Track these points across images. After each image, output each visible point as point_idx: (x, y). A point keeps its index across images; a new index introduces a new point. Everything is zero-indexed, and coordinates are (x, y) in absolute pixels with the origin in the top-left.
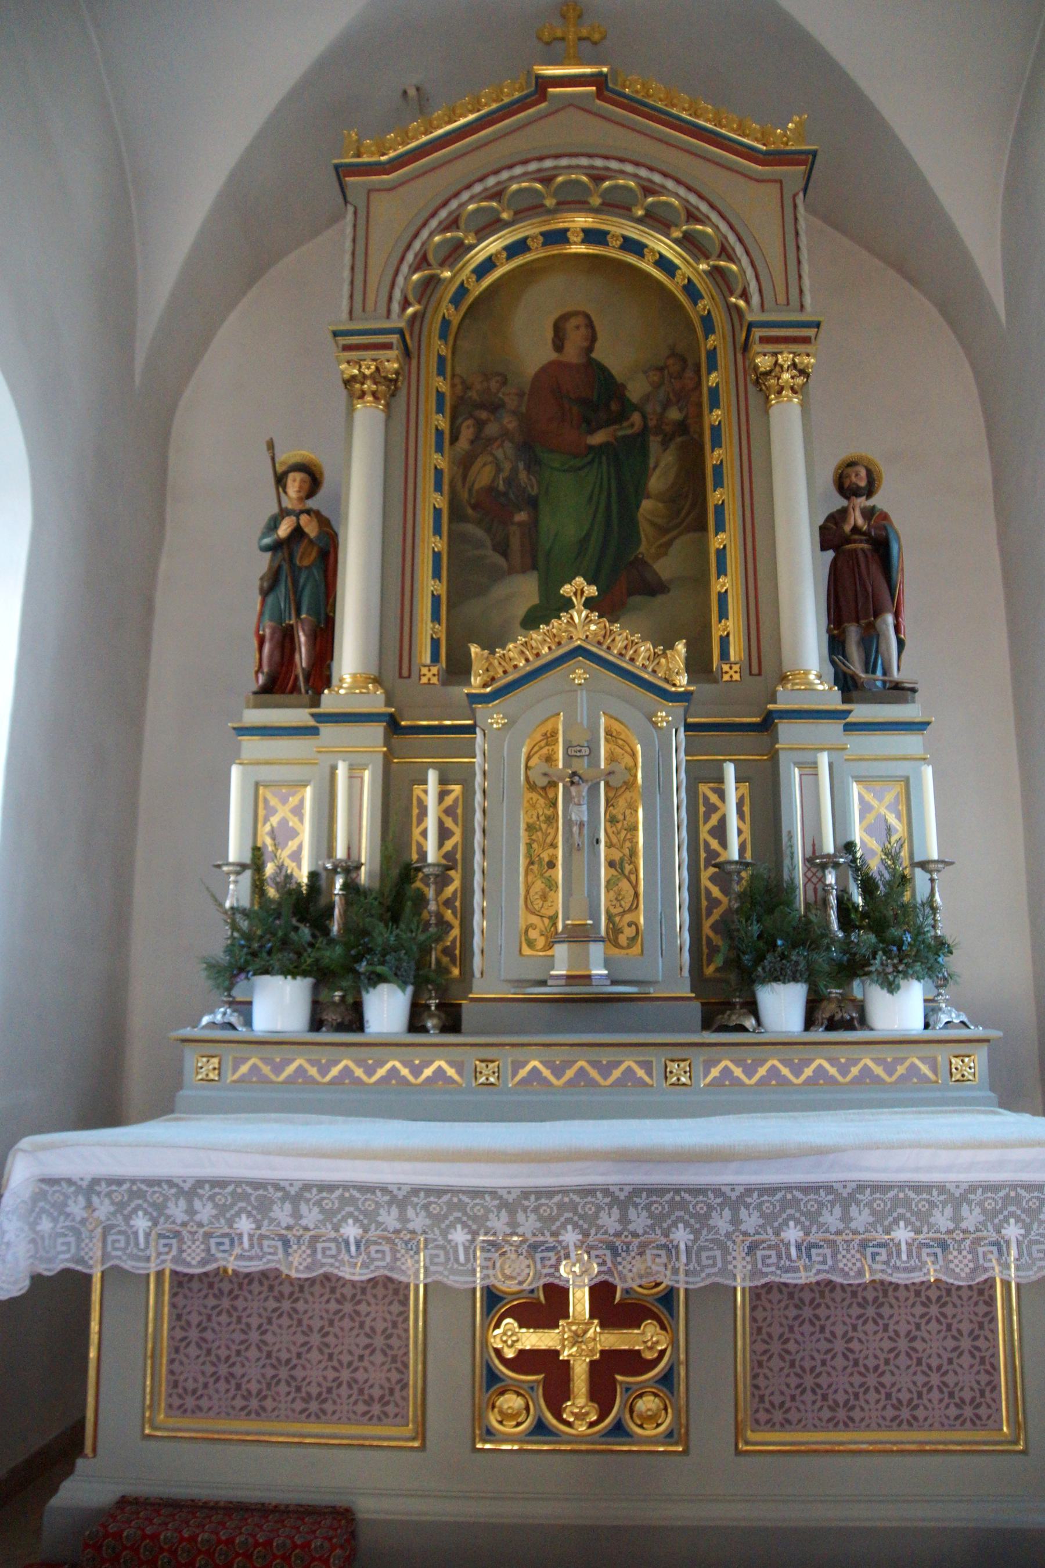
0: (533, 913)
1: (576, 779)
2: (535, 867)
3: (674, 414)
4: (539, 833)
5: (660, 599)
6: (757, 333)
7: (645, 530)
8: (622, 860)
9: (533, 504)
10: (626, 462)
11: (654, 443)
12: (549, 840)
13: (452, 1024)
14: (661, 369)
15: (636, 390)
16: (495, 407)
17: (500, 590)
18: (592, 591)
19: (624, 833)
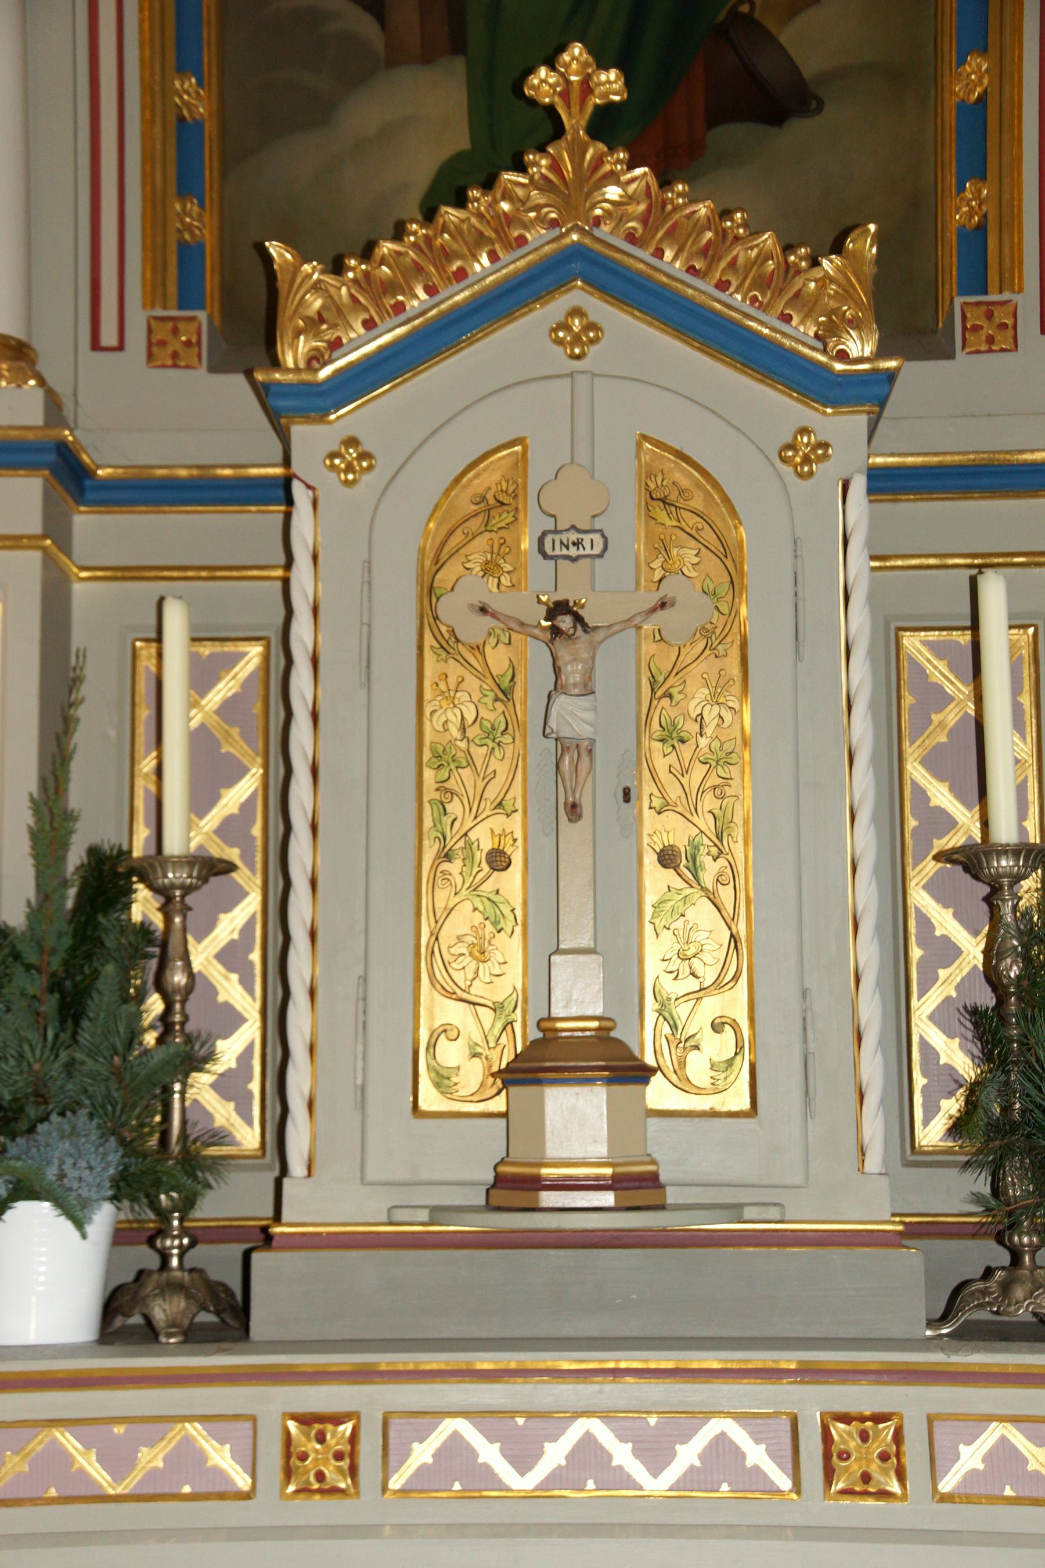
0: (450, 995)
1: (565, 622)
2: (455, 867)
4: (466, 773)
5: (798, 131)
8: (695, 847)
12: (493, 792)
13: (229, 1316)
17: (366, 112)
18: (611, 83)
19: (698, 772)
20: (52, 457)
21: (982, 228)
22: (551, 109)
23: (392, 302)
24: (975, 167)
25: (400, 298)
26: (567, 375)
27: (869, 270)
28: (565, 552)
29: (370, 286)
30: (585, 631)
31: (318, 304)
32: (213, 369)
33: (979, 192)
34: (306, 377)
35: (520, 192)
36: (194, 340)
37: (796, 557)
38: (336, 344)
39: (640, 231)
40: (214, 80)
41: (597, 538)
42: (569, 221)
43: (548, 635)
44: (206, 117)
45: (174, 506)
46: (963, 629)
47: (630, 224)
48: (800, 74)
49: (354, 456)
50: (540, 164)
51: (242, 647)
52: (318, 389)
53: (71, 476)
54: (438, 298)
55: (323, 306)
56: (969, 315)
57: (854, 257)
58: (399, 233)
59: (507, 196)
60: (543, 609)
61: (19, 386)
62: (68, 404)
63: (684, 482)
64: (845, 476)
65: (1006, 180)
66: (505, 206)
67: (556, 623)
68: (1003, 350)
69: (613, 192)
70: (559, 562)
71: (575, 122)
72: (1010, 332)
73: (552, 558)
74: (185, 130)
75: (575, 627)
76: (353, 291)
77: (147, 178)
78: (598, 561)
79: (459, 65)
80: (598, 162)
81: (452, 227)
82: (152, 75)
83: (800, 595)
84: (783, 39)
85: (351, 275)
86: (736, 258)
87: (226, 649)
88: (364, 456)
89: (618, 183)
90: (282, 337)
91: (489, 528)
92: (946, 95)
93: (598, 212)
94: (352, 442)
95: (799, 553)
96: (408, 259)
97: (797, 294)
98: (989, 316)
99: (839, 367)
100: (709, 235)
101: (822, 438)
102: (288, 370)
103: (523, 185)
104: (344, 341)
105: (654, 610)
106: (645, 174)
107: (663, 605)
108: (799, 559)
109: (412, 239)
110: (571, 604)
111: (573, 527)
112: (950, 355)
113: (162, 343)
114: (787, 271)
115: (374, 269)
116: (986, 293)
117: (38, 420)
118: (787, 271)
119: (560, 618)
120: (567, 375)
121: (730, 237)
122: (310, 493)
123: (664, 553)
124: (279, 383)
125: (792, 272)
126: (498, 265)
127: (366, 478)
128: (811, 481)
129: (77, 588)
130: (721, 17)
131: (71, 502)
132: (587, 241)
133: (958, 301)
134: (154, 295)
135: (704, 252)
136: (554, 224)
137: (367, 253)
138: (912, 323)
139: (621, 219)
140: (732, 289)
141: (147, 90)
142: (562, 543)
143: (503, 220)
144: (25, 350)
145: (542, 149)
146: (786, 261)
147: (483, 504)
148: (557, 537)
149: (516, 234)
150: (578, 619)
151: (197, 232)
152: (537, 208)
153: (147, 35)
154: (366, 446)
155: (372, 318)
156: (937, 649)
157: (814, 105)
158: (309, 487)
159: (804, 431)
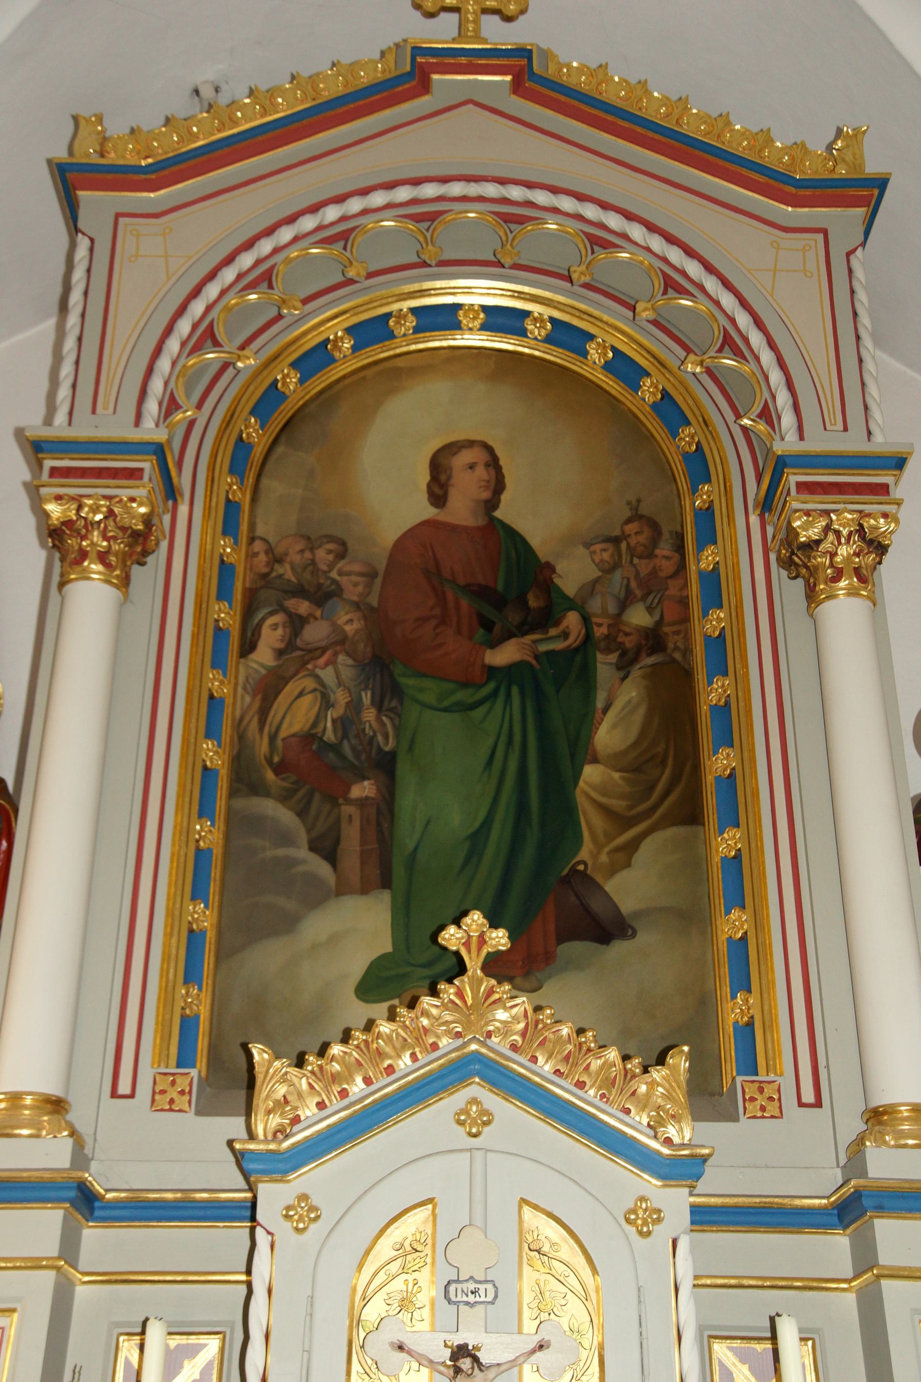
1: (465, 1364)
3: (639, 617)
5: (619, 948)
6: (793, 478)
7: (591, 821)
9: (385, 766)
10: (555, 696)
11: (604, 665)
14: (616, 541)
15: (573, 573)
16: (323, 595)
17: (319, 925)
18: (499, 939)
20: (73, 1194)
21: (750, 1024)
22: (457, 954)
23: (339, 1089)
24: (743, 983)
25: (345, 1086)
26: (467, 1150)
27: (683, 1078)
28: (465, 1299)
29: (323, 1076)
30: (481, 1370)
31: (282, 1090)
32: (199, 1113)
33: (747, 1001)
34: (272, 1146)
35: (434, 1011)
36: (187, 1090)
37: (640, 1302)
38: (296, 1120)
39: (520, 1043)
40: (216, 904)
41: (489, 1287)
42: (471, 1033)
43: (451, 1372)
44: (209, 928)
45: (160, 1222)
46: (759, 1339)
47: (513, 1038)
48: (619, 911)
49: (304, 1213)
50: (448, 991)
51: (203, 1339)
52: (281, 1157)
53: (86, 1202)
54: (373, 1088)
55: (287, 1092)
56: (747, 1090)
57: (674, 1068)
58: (346, 1038)
59: (425, 1013)
60: (448, 1352)
61: (55, 1137)
62: (89, 1141)
63: (555, 1238)
64: (674, 1236)
65: (765, 996)
66: (425, 1022)
67: (458, 1364)
68: (772, 1117)
69: (502, 1015)
70: (462, 1307)
71: (474, 964)
72: (776, 1103)
73: (455, 1303)
74: (194, 937)
75: (473, 1368)
76: (310, 1081)
77: (164, 973)
78: (489, 1306)
79: (386, 896)
80: (490, 992)
81: (385, 1036)
82: (174, 903)
83: (644, 1336)
84: (607, 888)
85: (309, 1068)
86: (589, 1065)
87: (190, 1341)
88: (313, 1209)
89: (505, 1009)
90: (256, 1115)
91: (405, 1270)
92: (719, 932)
93: (491, 1028)
94: (304, 1197)
95: (642, 1300)
96: (353, 1059)
97: (634, 1093)
98: (761, 1090)
99: (666, 1151)
100: (570, 1047)
101: (656, 1205)
102: (261, 1142)
103: (437, 1006)
104: (302, 1118)
105: (533, 1352)
106: (524, 1002)
107: (541, 1347)
108: (642, 1304)
109: (355, 1043)
110: (470, 1347)
111: (472, 1278)
112: (736, 1119)
113: (163, 1092)
114: (626, 1075)
115: (327, 1064)
116: (757, 1075)
117: (66, 1164)
118: (626, 1075)
119: (461, 1361)
120: (467, 1150)
121: (584, 1049)
122: (270, 1237)
123: (540, 1296)
124: (252, 1151)
125: (629, 1076)
126: (418, 1064)
127: (313, 1227)
128: (649, 1240)
129: (80, 1290)
130: (565, 872)
131: (83, 1221)
132: (484, 1050)
133: (739, 1079)
134: (161, 1056)
135: (567, 1059)
136: (458, 1035)
137: (322, 1052)
138: (708, 1096)
139: (506, 1033)
140: (586, 1088)
141: (170, 913)
142: (463, 1291)
143: (422, 1031)
144: (62, 1104)
145: (450, 981)
146: (625, 1069)
147: (401, 1251)
148: (459, 1286)
149: (431, 1041)
150: (476, 1359)
151: (195, 1008)
152: (446, 1023)
153: (174, 878)
154: (315, 1201)
155: (323, 1100)
156: (743, 1357)
157: (630, 932)
158: (269, 1233)
159: (643, 1199)
